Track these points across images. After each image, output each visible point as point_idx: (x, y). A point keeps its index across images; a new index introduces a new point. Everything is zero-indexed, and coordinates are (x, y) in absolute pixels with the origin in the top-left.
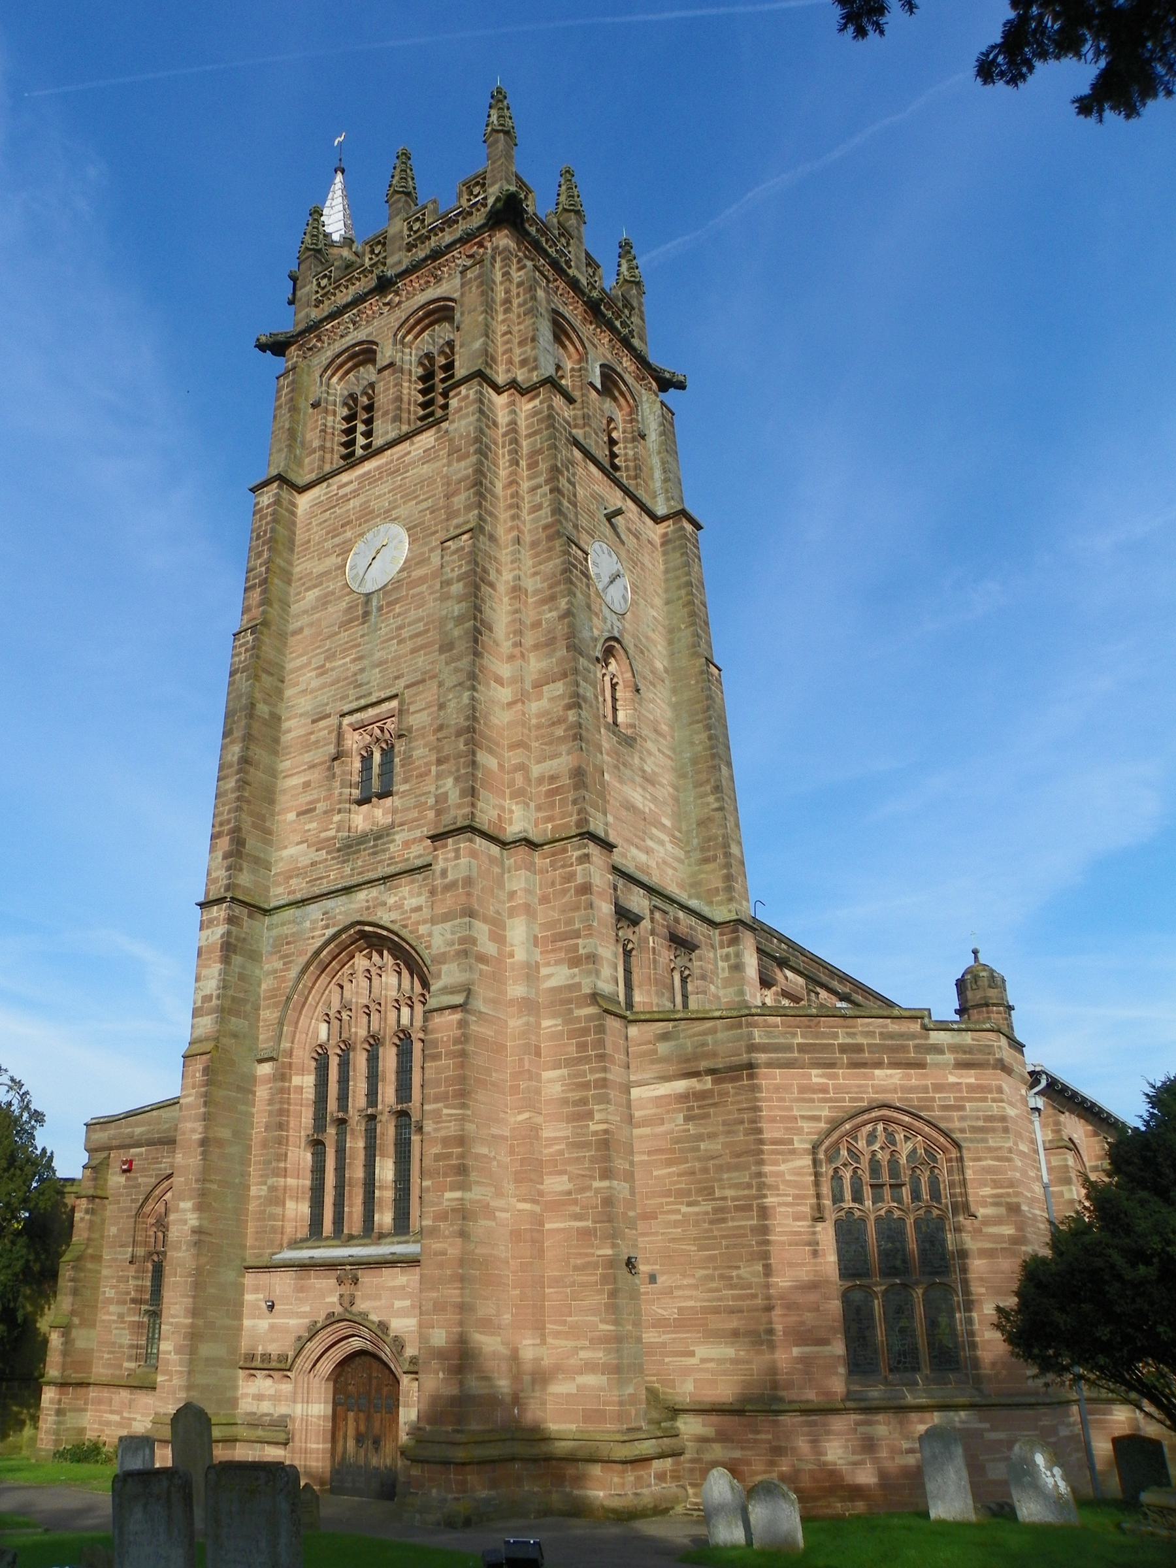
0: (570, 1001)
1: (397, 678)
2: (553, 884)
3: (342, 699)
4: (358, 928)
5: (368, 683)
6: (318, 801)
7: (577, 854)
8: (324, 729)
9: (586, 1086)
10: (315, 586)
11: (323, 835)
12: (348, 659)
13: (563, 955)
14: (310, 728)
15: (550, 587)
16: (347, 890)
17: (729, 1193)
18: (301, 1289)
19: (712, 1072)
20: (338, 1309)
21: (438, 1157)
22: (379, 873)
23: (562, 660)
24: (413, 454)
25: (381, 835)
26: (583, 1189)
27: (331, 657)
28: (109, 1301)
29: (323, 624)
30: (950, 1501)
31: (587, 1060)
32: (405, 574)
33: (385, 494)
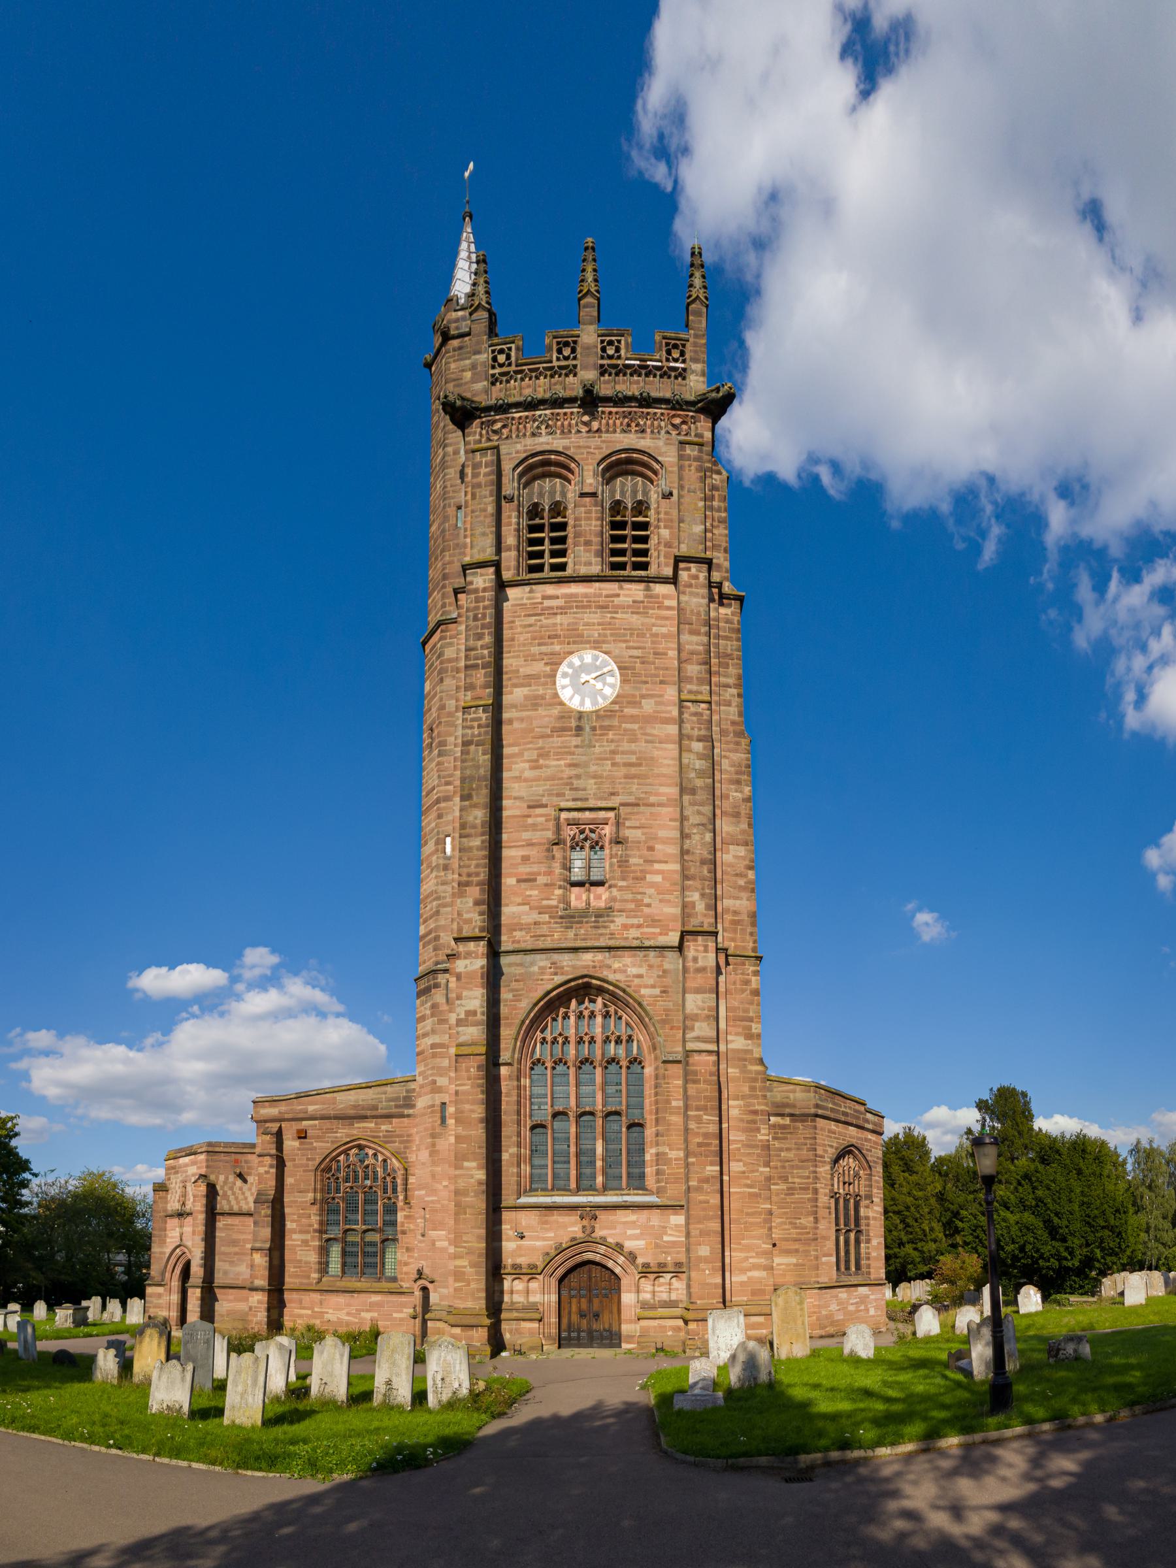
0: (745, 1060)
1: (613, 794)
2: (735, 983)
3: (558, 795)
4: (586, 980)
5: (584, 789)
6: (539, 874)
7: (752, 968)
8: (541, 816)
9: (755, 1112)
10: (522, 685)
11: (545, 903)
12: (562, 762)
13: (740, 1030)
14: (527, 812)
15: (737, 773)
16: (575, 950)
17: (797, 1180)
18: (546, 1223)
19: (791, 1115)
20: (580, 1235)
21: (699, 1145)
22: (602, 942)
23: (743, 832)
24: (622, 598)
25: (604, 914)
26: (753, 1171)
27: (543, 754)
28: (294, 1231)
29: (535, 723)
30: (40, 1309)
31: (756, 1097)
32: (617, 707)
33: (594, 624)
